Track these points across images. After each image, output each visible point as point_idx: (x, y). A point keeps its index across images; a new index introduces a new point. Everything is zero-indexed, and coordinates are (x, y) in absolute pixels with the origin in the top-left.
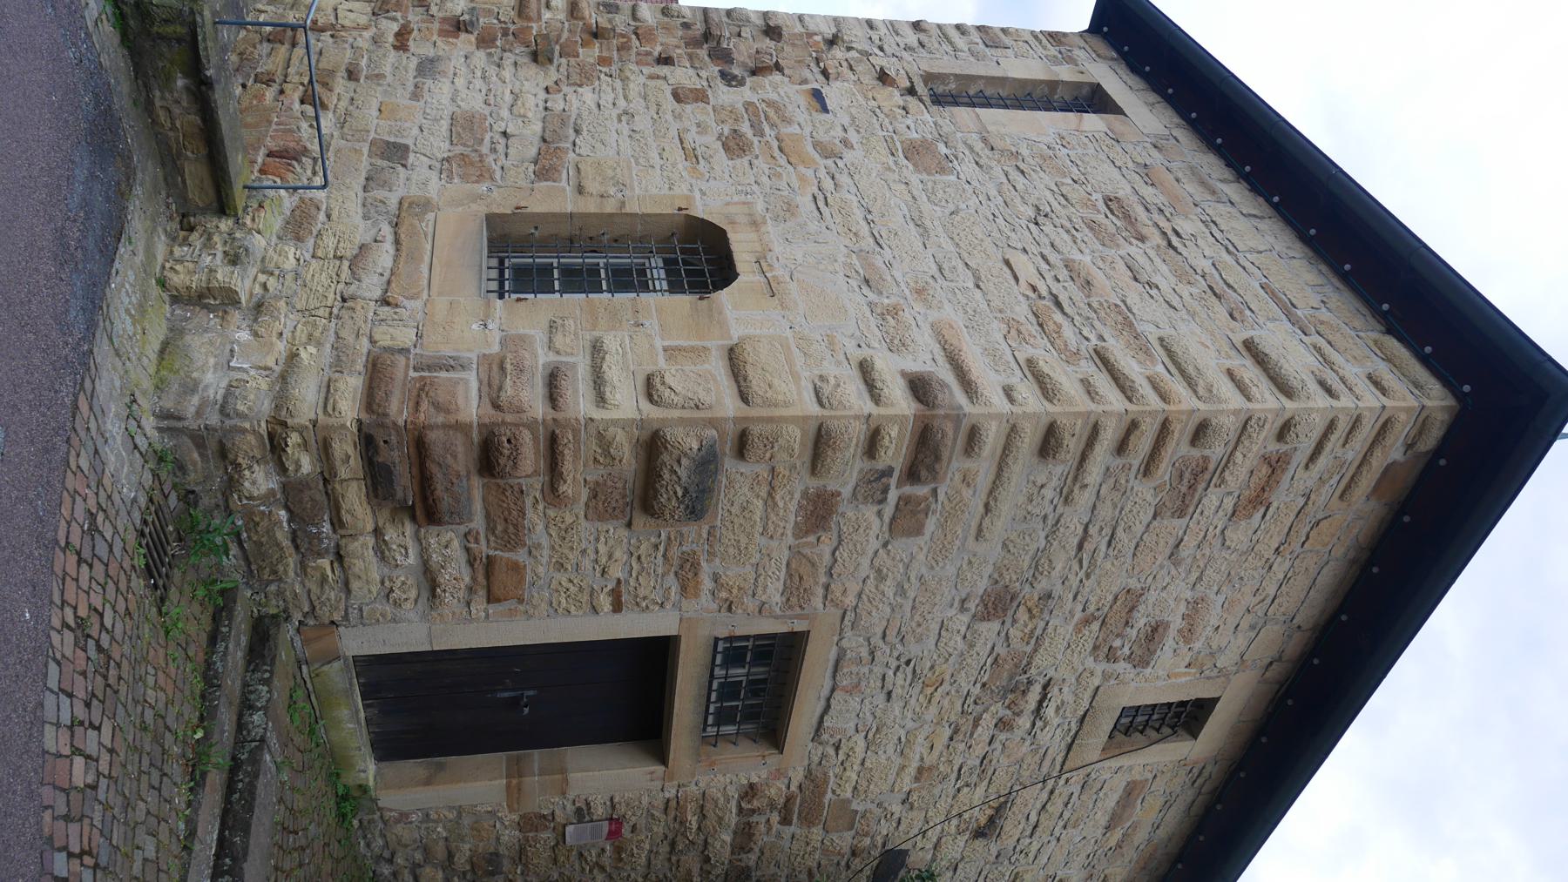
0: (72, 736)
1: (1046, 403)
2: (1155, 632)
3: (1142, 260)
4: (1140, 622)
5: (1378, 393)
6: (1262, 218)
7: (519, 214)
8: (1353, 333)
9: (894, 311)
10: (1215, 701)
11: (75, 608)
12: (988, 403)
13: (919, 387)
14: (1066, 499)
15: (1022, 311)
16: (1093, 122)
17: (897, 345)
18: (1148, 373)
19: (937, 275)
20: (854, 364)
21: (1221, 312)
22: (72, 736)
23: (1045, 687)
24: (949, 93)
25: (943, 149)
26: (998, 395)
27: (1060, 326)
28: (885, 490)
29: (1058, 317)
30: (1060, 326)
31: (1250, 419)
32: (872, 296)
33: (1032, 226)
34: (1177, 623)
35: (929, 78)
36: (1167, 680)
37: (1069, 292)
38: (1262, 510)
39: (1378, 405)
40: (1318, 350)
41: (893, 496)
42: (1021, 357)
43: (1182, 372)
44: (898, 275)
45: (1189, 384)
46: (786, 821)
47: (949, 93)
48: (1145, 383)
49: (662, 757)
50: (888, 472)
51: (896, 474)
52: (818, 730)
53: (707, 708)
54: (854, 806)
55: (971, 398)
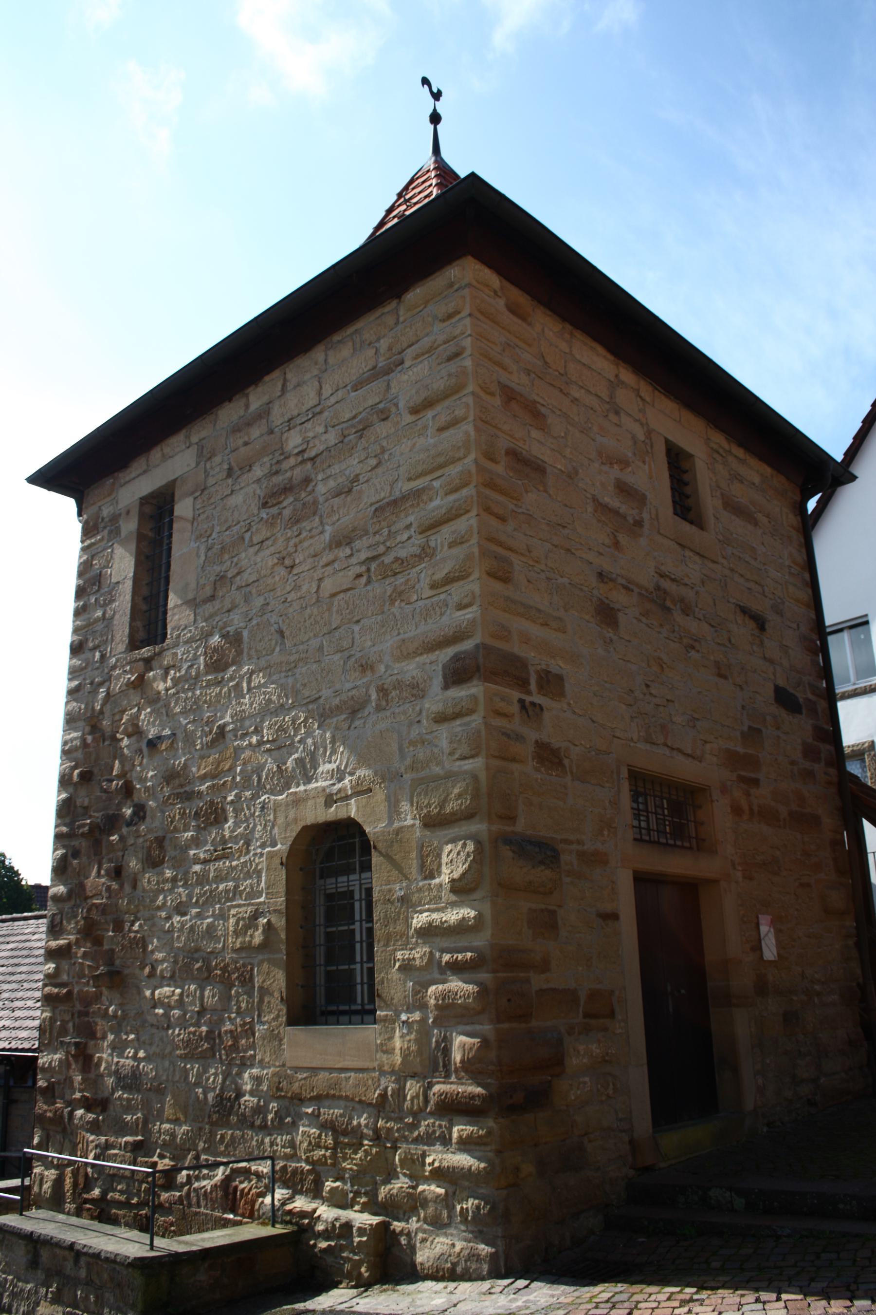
0: (769, 1302)
1: (471, 578)
2: (623, 489)
3: (332, 483)
4: (614, 502)
5: (458, 317)
6: (285, 381)
7: (288, 1001)
8: (400, 327)
9: (383, 691)
10: (667, 442)
11: (674, 1308)
12: (473, 622)
13: (457, 674)
14: (537, 562)
15: (378, 589)
16: (183, 508)
17: (417, 691)
18: (441, 493)
19: (346, 654)
20: (435, 727)
21: (382, 429)
22: (769, 1302)
23: (661, 576)
24: (150, 626)
25: (216, 639)
26: (461, 612)
27: (397, 559)
28: (533, 704)
29: (388, 559)
30: (397, 559)
31: (481, 419)
32: (370, 708)
33: (295, 571)
34: (615, 472)
35: (134, 644)
36: (653, 480)
37: (363, 548)
38: (538, 406)
39: (468, 321)
40: (417, 357)
41: (537, 699)
42: (428, 593)
43: (441, 466)
44: (348, 686)
45: (453, 462)
46: (756, 782)
47: (150, 626)
48: (452, 498)
49: (712, 882)
50: (521, 702)
51: (523, 696)
52: (694, 758)
53: (670, 845)
54: (745, 729)
55: (469, 637)
